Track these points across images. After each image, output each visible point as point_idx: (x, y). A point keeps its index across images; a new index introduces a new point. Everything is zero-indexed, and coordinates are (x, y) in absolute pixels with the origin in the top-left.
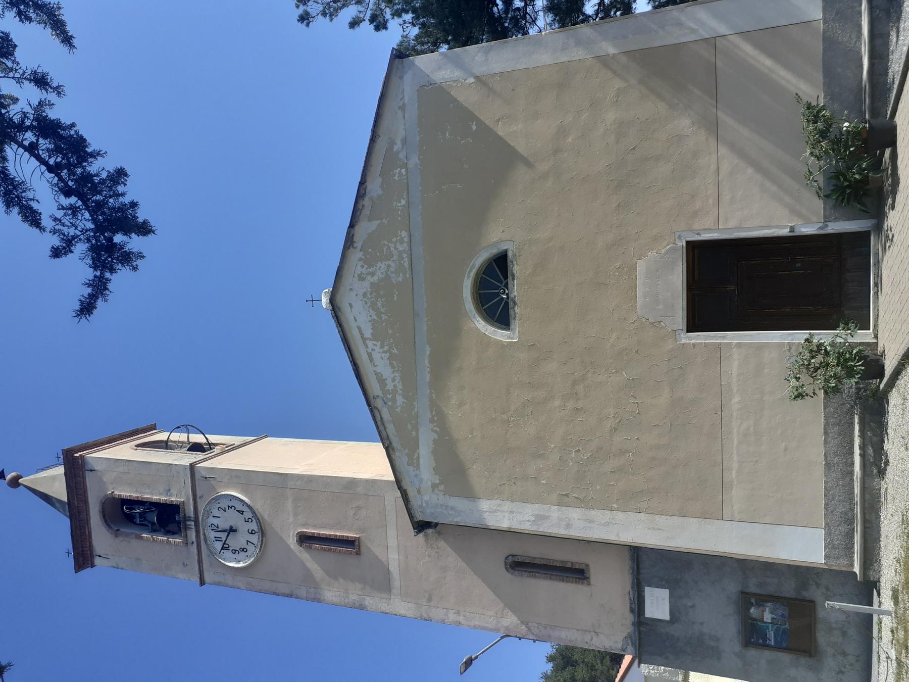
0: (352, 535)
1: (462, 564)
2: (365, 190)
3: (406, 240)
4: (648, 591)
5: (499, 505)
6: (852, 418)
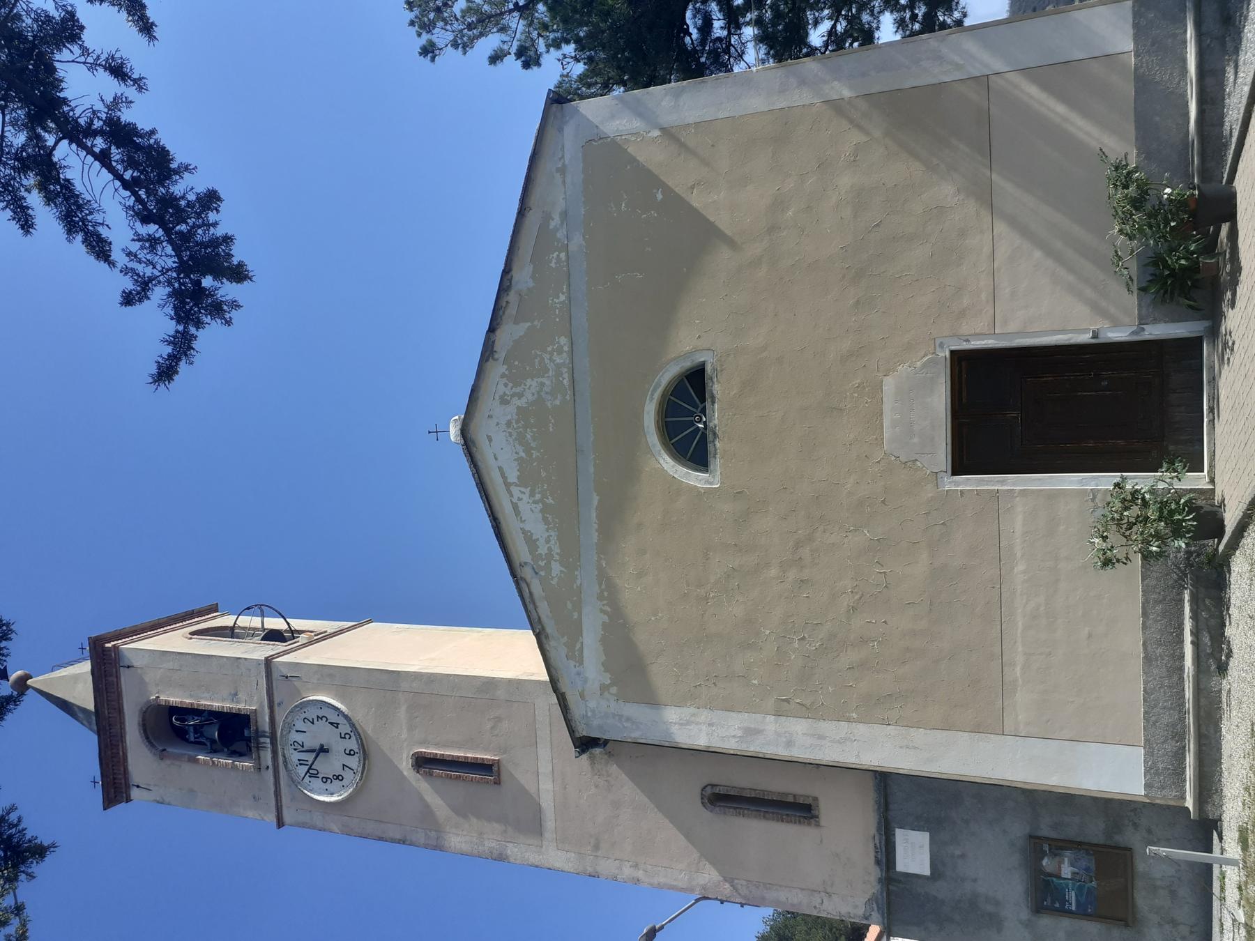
0: (489, 757)
1: (641, 798)
3: (566, 348)
5: (694, 715)
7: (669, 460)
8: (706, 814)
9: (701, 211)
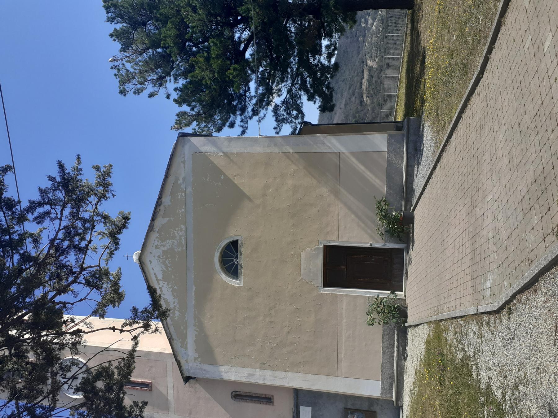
0: (147, 381)
1: (208, 396)
2: (161, 202)
3: (184, 229)
4: (302, 408)
5: (230, 369)
6: (394, 332)
7: (224, 275)
8: (232, 401)
9: (238, 185)
